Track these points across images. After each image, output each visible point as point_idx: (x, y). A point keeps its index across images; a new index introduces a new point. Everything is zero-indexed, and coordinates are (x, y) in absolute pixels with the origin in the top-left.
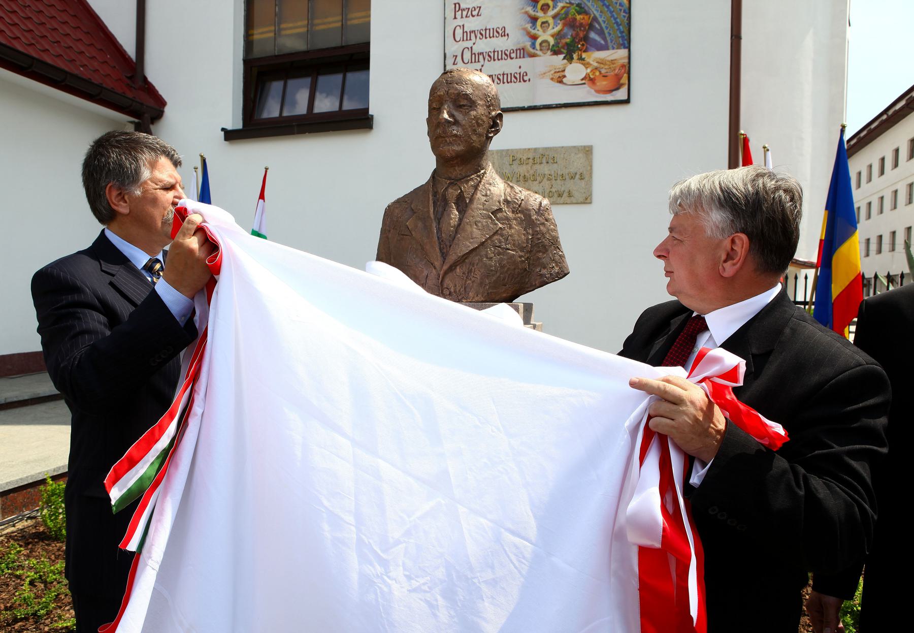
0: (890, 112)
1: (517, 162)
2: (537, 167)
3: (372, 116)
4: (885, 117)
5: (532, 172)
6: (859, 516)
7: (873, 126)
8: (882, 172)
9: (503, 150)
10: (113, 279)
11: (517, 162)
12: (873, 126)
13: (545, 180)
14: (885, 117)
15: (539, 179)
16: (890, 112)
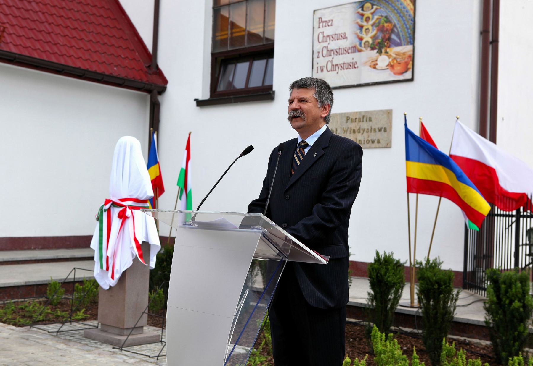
5: (358, 127)
13: (365, 132)
15: (362, 131)
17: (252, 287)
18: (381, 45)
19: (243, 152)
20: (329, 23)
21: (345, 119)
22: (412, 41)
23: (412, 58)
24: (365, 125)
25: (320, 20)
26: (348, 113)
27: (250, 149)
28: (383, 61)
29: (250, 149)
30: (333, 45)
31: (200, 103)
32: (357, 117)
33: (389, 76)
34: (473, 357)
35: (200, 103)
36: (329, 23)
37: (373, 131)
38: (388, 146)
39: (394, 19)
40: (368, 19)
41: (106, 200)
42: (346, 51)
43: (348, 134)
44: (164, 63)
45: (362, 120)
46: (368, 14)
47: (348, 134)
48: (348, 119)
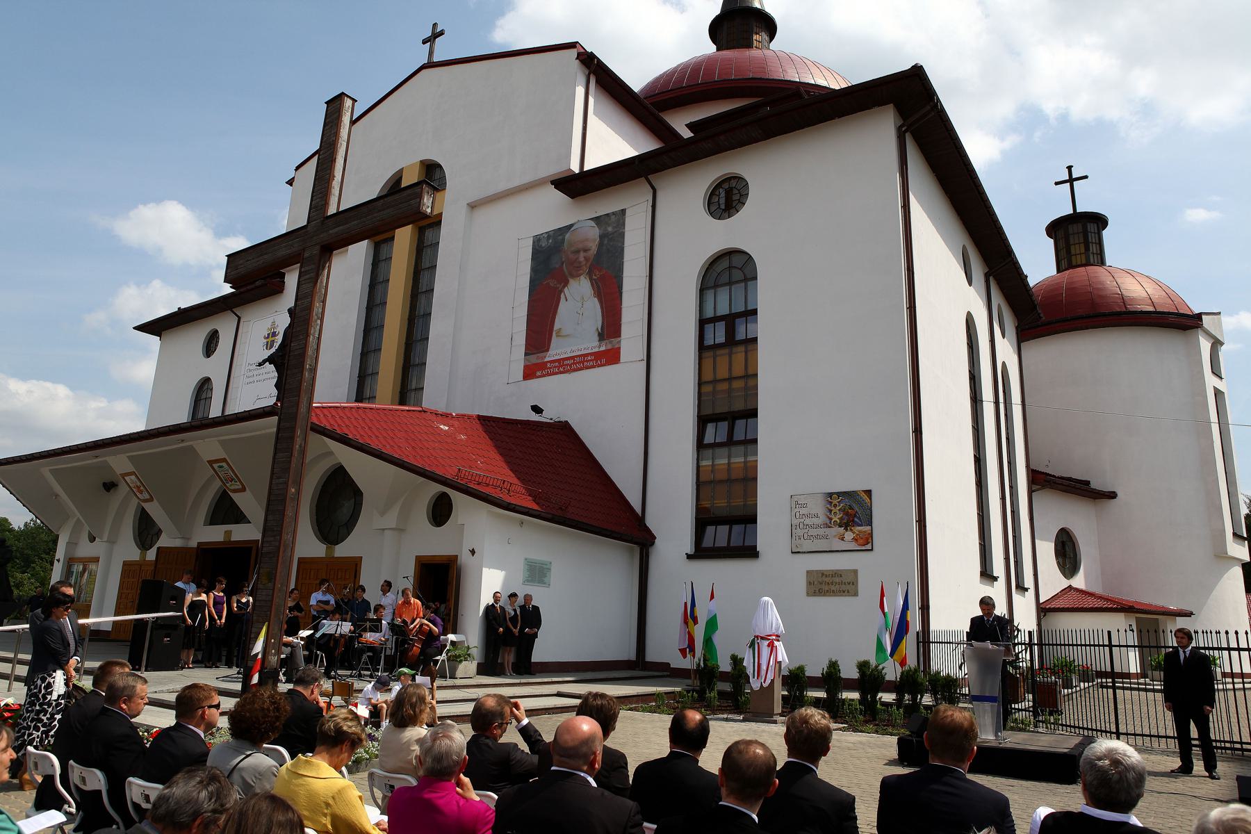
17: (707, 721)
18: (847, 523)
19: (907, 623)
20: (804, 506)
22: (870, 523)
23: (871, 535)
24: (837, 580)
25: (797, 503)
27: (712, 597)
28: (849, 536)
29: (712, 597)
30: (808, 521)
33: (853, 546)
34: (1156, 673)
35: (689, 557)
36: (804, 506)
39: (856, 508)
40: (835, 506)
42: (819, 526)
44: (651, 522)
46: (835, 502)
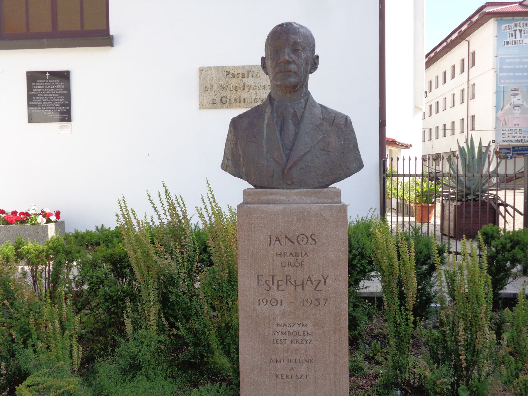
0: (449, 41)
1: (230, 75)
2: (245, 80)
3: (113, 36)
4: (445, 44)
5: (241, 84)
6: (476, 156)
7: (438, 50)
8: (445, 82)
9: (219, 67)
10: (428, 90)
11: (230, 75)
12: (438, 50)
13: (251, 90)
14: (445, 44)
15: (247, 89)
16: (449, 41)
21: (224, 74)
26: (226, 67)
31: (196, 207)
32: (240, 72)
37: (262, 88)
38: (64, 76)
41: (68, 73)
43: (228, 92)
45: (246, 75)
47: (228, 92)
48: (228, 73)
